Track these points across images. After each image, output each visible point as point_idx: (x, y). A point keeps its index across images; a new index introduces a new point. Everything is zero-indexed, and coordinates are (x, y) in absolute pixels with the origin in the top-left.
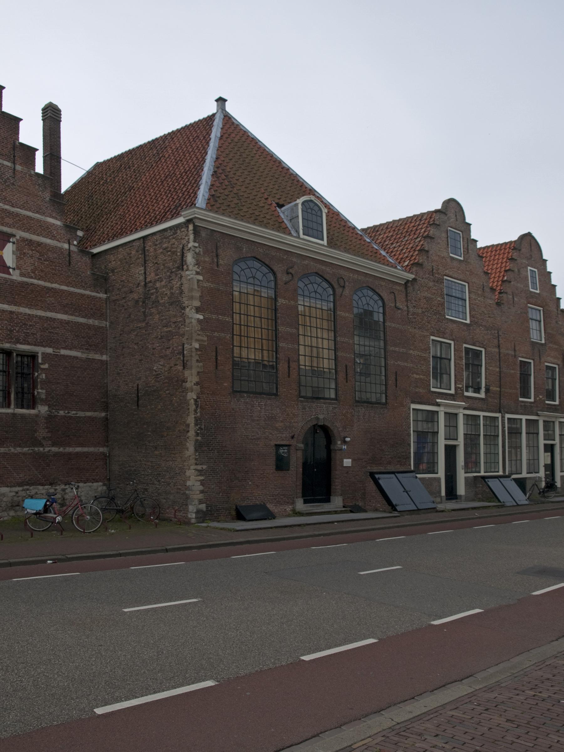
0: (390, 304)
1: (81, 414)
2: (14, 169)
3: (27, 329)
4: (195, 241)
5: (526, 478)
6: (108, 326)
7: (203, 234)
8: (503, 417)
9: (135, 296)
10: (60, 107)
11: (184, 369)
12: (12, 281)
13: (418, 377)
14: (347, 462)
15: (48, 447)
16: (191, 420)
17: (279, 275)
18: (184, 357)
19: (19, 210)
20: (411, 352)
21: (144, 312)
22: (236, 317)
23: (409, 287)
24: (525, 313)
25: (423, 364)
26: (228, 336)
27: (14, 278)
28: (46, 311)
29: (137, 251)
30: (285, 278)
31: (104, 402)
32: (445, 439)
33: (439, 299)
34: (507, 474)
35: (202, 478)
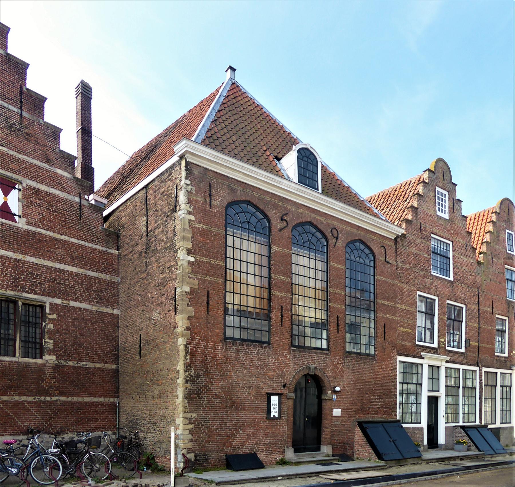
0: (380, 258)
1: (90, 365)
2: (21, 114)
3: (34, 278)
5: (500, 428)
6: (120, 281)
7: (196, 172)
8: (480, 370)
9: (139, 248)
11: (175, 314)
12: (18, 228)
13: (405, 330)
14: (337, 412)
15: (56, 396)
16: (181, 367)
17: (273, 222)
18: (175, 301)
19: (25, 157)
20: (399, 306)
21: (146, 262)
23: (398, 242)
24: (502, 273)
25: (409, 318)
26: (221, 281)
27: (20, 225)
28: (54, 262)
29: (141, 202)
31: (115, 354)
32: (428, 391)
33: (426, 256)
34: (483, 424)
35: (191, 426)
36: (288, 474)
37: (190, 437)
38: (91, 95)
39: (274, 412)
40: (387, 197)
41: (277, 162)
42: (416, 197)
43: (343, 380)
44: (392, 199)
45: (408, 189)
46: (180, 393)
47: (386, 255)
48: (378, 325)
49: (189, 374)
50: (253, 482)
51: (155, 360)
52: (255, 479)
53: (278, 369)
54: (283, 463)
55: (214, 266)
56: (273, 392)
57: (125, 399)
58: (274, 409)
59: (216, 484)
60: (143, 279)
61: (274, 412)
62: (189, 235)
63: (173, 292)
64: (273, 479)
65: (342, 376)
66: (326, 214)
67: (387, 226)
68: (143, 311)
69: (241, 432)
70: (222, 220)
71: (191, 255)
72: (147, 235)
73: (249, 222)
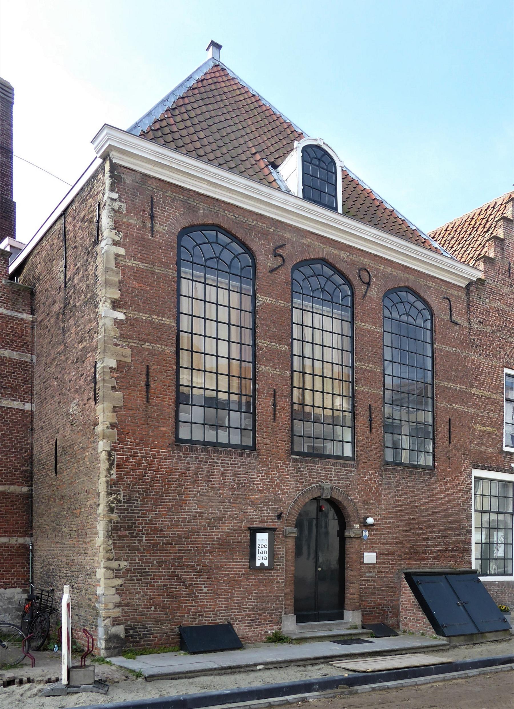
0: (442, 316)
4: (112, 190)
6: (34, 361)
7: (128, 180)
10: (13, 84)
11: (96, 404)
13: (484, 428)
14: (370, 557)
16: (102, 487)
17: (260, 258)
18: (95, 384)
20: (474, 390)
22: (185, 321)
26: (170, 350)
30: (271, 263)
31: (26, 471)
35: (119, 582)
36: (274, 660)
37: (117, 599)
38: (13, 99)
39: (262, 558)
40: (459, 229)
41: (273, 170)
42: (501, 223)
43: (380, 506)
44: (466, 231)
45: (491, 215)
46: (101, 528)
47: (451, 312)
48: (438, 421)
49: (115, 499)
50: (212, 675)
51: (72, 477)
52: (215, 669)
53: (269, 489)
54: (278, 639)
55: (157, 327)
56: (261, 525)
57: (39, 538)
58: (262, 552)
59: (146, 678)
60: (59, 353)
61: (262, 558)
62: (116, 279)
63: (93, 370)
64: (248, 669)
65: (379, 501)
66: (350, 246)
67: (453, 267)
68: (59, 403)
69: (205, 590)
70: (173, 254)
71: (119, 310)
72: (65, 287)
73: (218, 258)
